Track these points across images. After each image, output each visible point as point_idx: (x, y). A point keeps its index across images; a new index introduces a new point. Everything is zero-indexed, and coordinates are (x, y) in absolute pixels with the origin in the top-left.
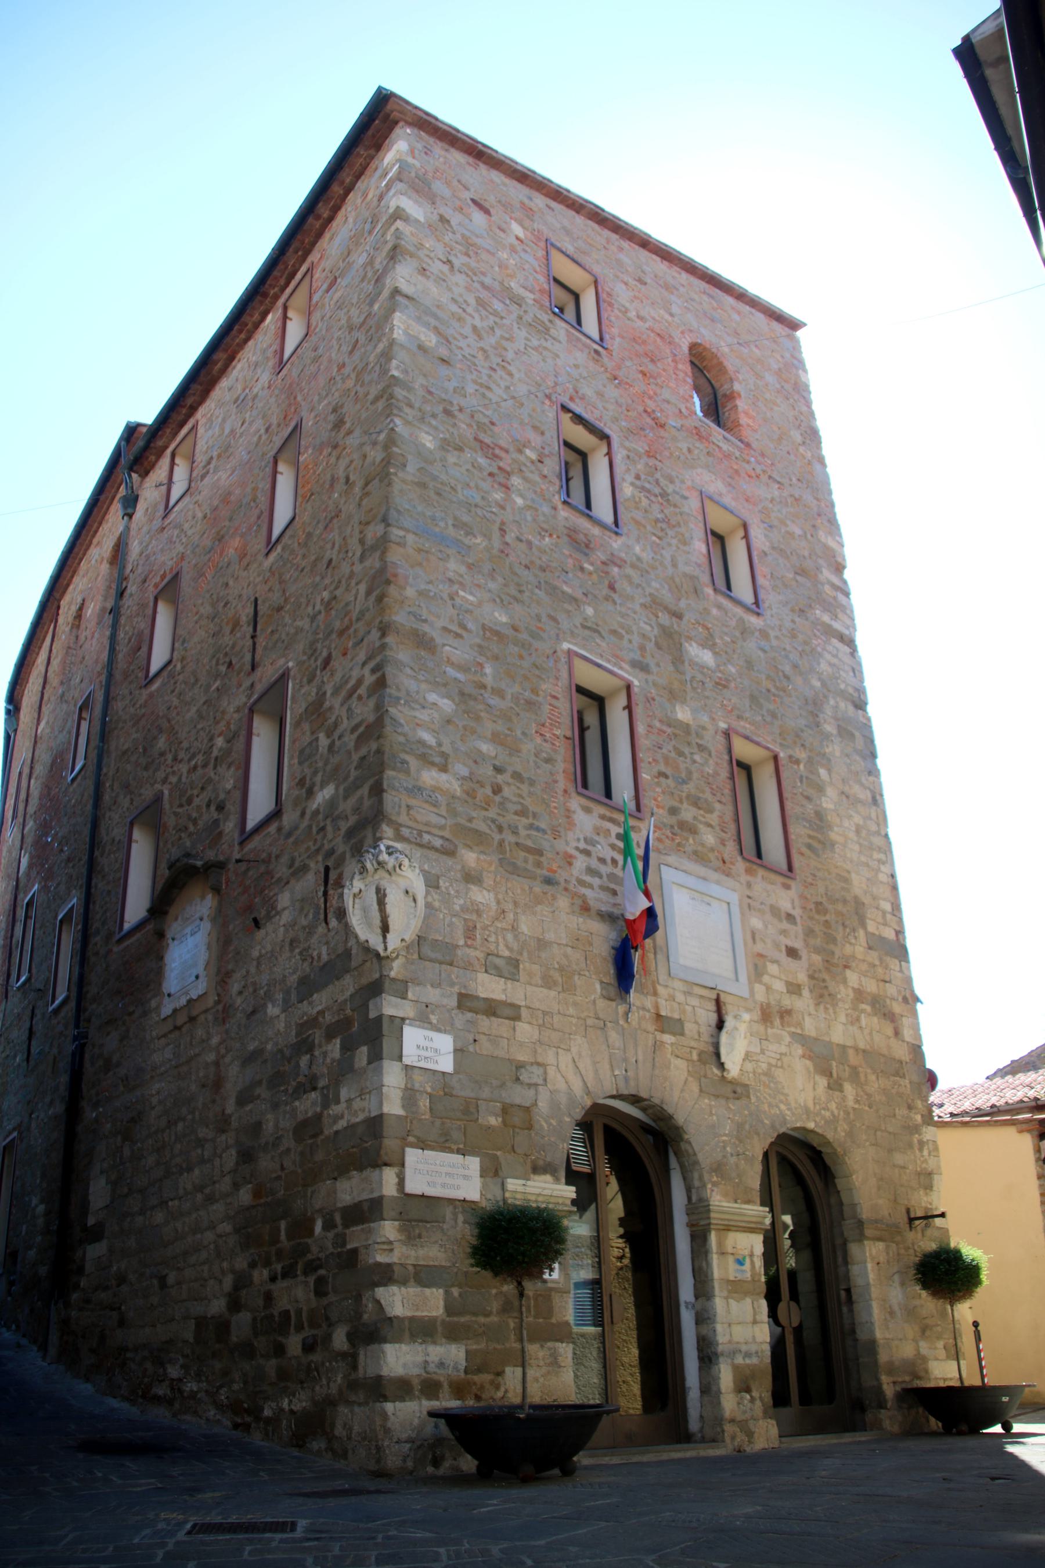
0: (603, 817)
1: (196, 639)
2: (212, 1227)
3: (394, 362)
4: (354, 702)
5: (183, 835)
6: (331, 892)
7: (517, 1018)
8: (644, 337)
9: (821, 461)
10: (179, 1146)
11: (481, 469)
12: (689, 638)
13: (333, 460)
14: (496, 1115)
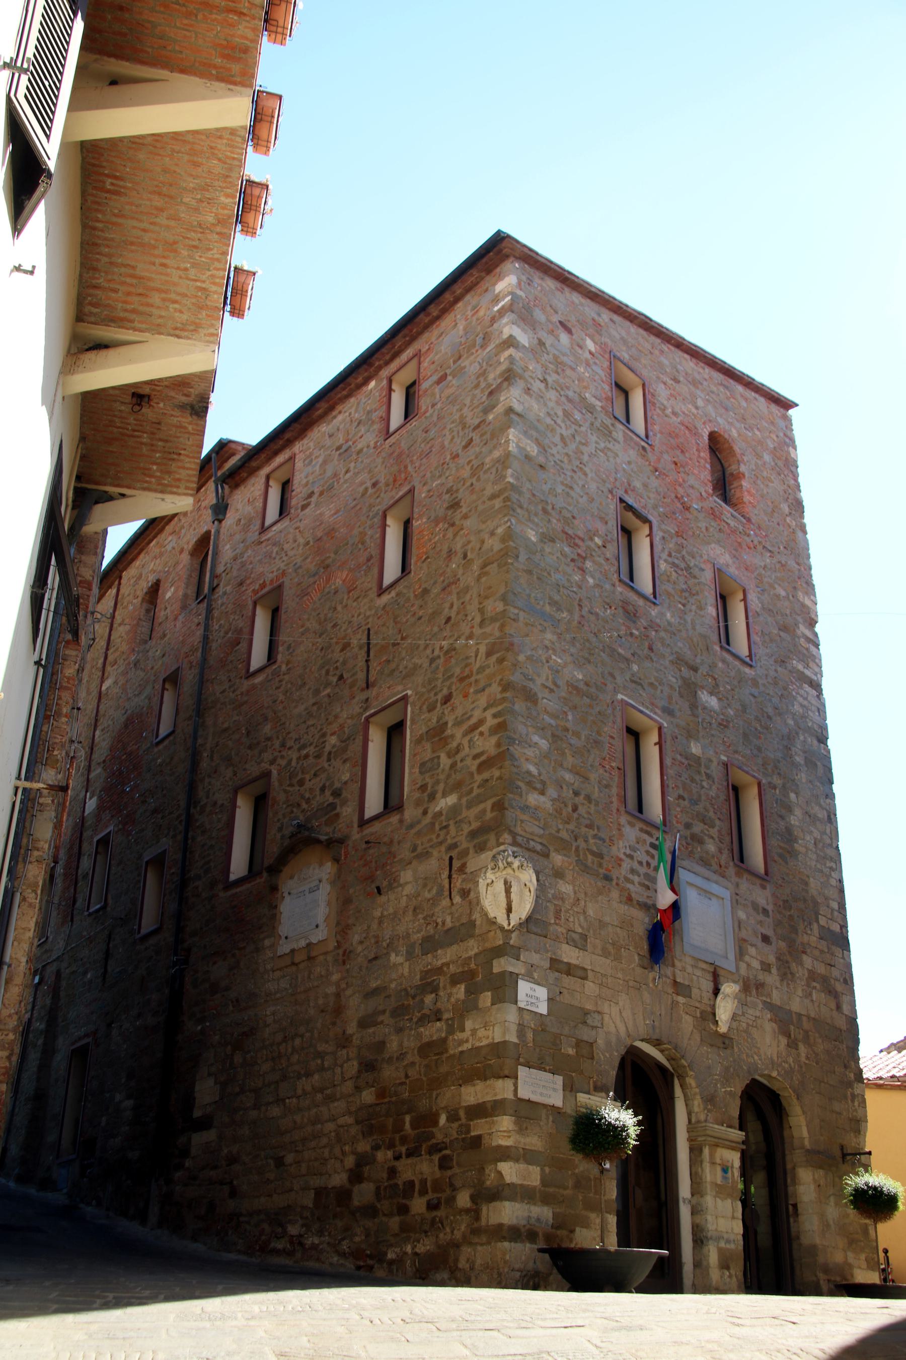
0: (641, 830)
1: (302, 648)
2: (333, 1119)
3: (510, 471)
4: (476, 735)
5: (295, 810)
6: (454, 876)
7: (585, 978)
8: (677, 431)
9: (803, 529)
10: (297, 1057)
11: (565, 556)
12: (702, 687)
13: (450, 535)
14: (573, 1048)
